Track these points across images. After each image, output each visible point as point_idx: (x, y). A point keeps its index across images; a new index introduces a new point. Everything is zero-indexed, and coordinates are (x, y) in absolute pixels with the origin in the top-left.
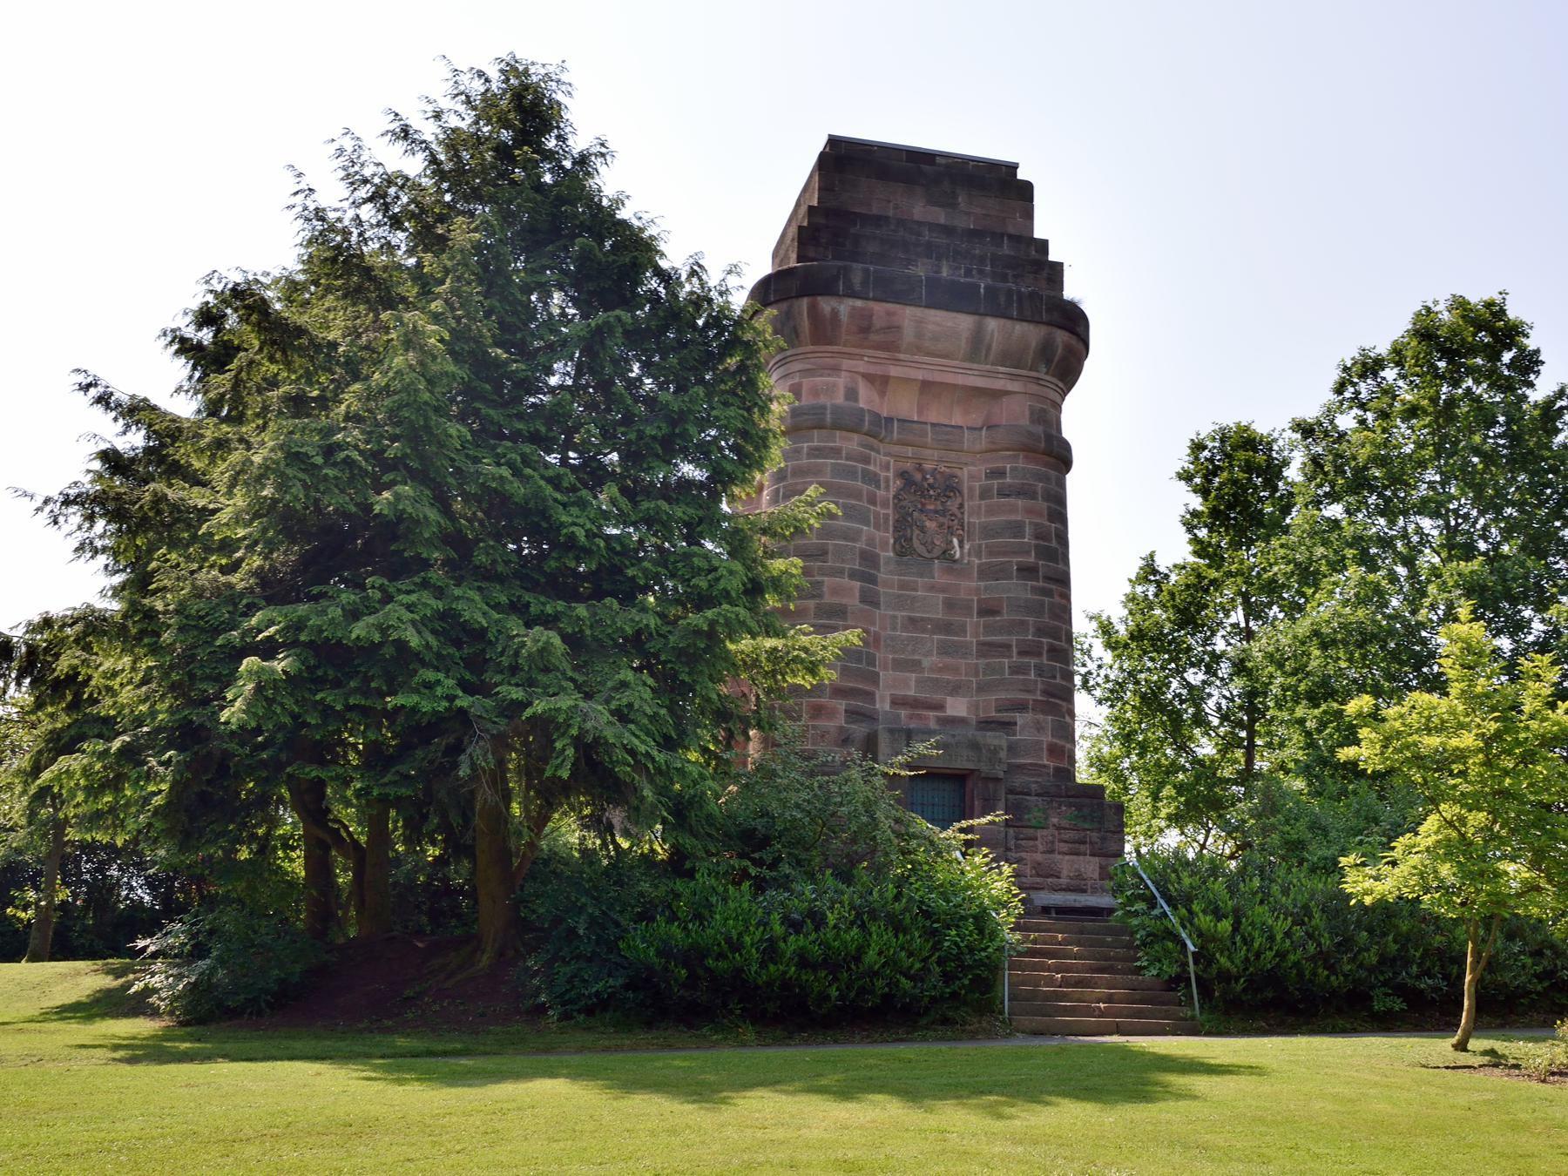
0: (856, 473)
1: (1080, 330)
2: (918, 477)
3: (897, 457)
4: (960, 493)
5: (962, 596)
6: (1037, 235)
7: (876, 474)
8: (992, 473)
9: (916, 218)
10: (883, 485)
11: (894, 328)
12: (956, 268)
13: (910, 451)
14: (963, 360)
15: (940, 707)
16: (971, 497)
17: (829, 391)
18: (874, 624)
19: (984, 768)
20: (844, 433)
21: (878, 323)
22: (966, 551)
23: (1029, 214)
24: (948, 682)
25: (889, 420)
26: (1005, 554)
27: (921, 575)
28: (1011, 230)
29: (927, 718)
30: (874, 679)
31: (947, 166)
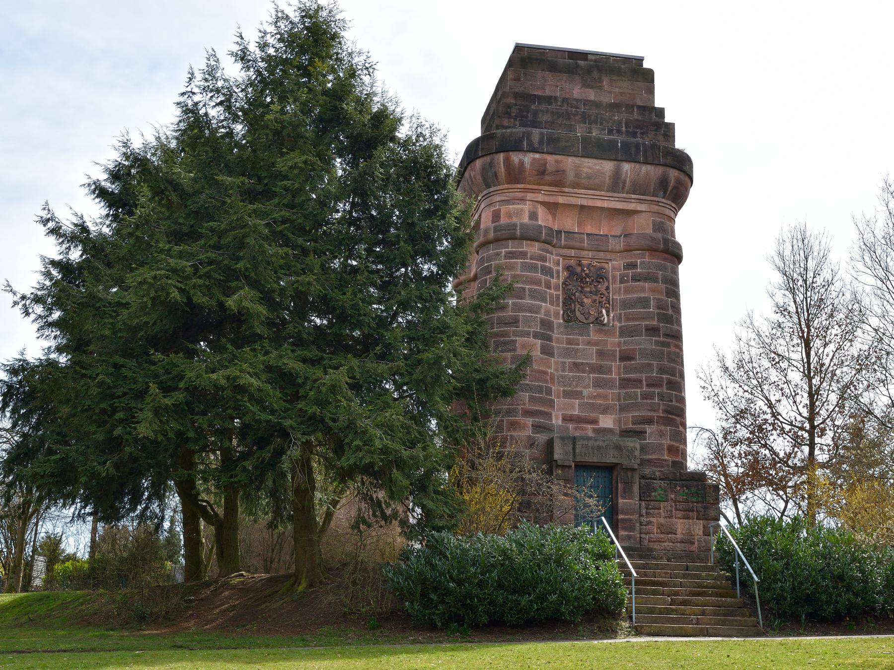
0: (538, 268)
1: (686, 168)
2: (579, 269)
3: (565, 257)
4: (608, 280)
5: (609, 348)
6: (657, 105)
7: (550, 268)
10: (555, 275)
11: (560, 172)
13: (572, 252)
14: (607, 191)
15: (595, 422)
16: (614, 282)
17: (519, 213)
18: (550, 367)
19: (625, 462)
20: (529, 242)
21: (550, 168)
22: (611, 318)
23: (651, 91)
24: (600, 405)
25: (559, 232)
28: (639, 103)
29: (586, 429)
30: (551, 404)
31: (596, 61)
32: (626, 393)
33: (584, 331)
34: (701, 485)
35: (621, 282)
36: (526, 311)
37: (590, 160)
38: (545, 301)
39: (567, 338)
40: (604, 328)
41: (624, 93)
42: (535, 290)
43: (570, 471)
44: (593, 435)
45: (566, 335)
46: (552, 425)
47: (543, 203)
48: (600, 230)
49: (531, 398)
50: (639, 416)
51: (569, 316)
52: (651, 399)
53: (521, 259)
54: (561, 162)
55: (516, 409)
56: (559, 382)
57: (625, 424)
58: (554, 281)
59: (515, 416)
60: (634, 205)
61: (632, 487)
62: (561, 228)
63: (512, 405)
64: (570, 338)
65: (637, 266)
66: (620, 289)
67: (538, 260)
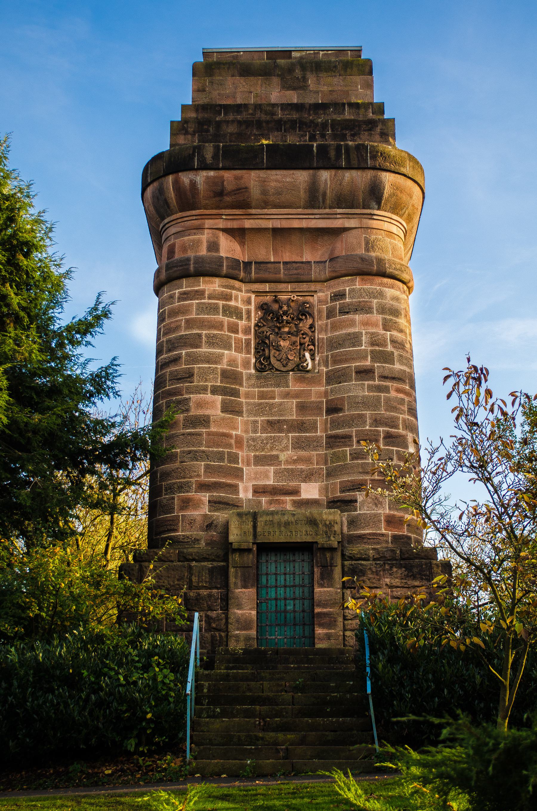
0: (218, 308)
2: (275, 307)
3: (258, 293)
4: (312, 316)
7: (237, 308)
8: (335, 295)
9: (273, 101)
11: (242, 190)
12: (302, 136)
13: (267, 287)
14: (305, 208)
15: (296, 492)
18: (236, 429)
19: (321, 540)
20: (207, 279)
21: (229, 186)
22: (317, 362)
24: (302, 471)
26: (202, 321)
27: (278, 386)
29: (284, 502)
30: (238, 474)
32: (334, 454)
33: (282, 382)
34: (426, 564)
35: (328, 318)
36: (203, 362)
37: (278, 172)
38: (229, 348)
39: (259, 392)
40: (309, 375)
41: (334, 91)
42: (215, 336)
43: (251, 556)
44: (292, 509)
45: (258, 387)
46: (241, 500)
47: (226, 231)
48: (301, 257)
49: (207, 467)
50: (348, 481)
51: (262, 364)
52: (362, 458)
53: (198, 299)
54: (241, 178)
55: (188, 482)
56: (249, 446)
57: (332, 493)
58: (242, 323)
59: (188, 492)
60: (340, 221)
61: (332, 571)
62: (252, 259)
63: (184, 478)
64: (263, 391)
65: (345, 295)
66: (327, 325)
67: (219, 300)
